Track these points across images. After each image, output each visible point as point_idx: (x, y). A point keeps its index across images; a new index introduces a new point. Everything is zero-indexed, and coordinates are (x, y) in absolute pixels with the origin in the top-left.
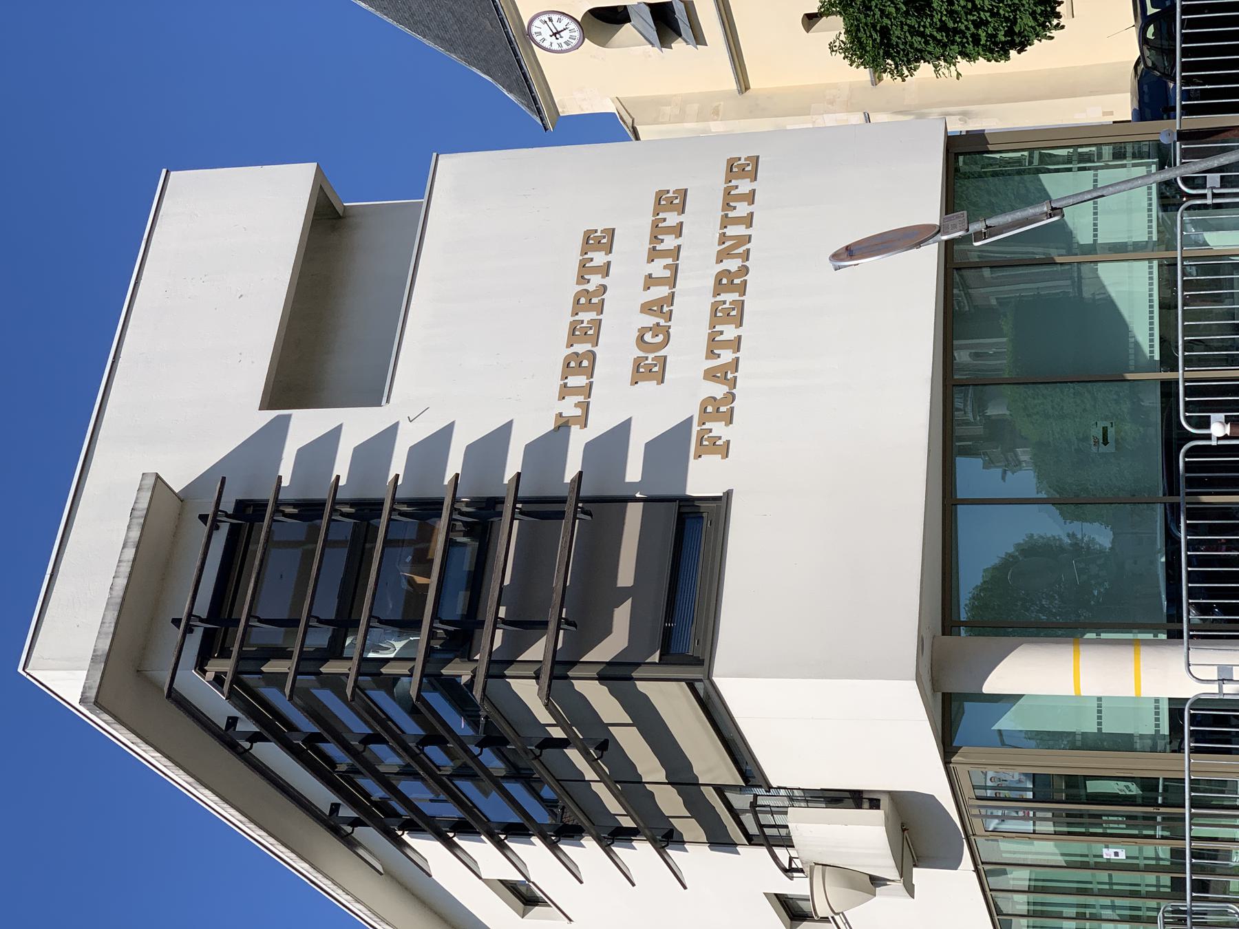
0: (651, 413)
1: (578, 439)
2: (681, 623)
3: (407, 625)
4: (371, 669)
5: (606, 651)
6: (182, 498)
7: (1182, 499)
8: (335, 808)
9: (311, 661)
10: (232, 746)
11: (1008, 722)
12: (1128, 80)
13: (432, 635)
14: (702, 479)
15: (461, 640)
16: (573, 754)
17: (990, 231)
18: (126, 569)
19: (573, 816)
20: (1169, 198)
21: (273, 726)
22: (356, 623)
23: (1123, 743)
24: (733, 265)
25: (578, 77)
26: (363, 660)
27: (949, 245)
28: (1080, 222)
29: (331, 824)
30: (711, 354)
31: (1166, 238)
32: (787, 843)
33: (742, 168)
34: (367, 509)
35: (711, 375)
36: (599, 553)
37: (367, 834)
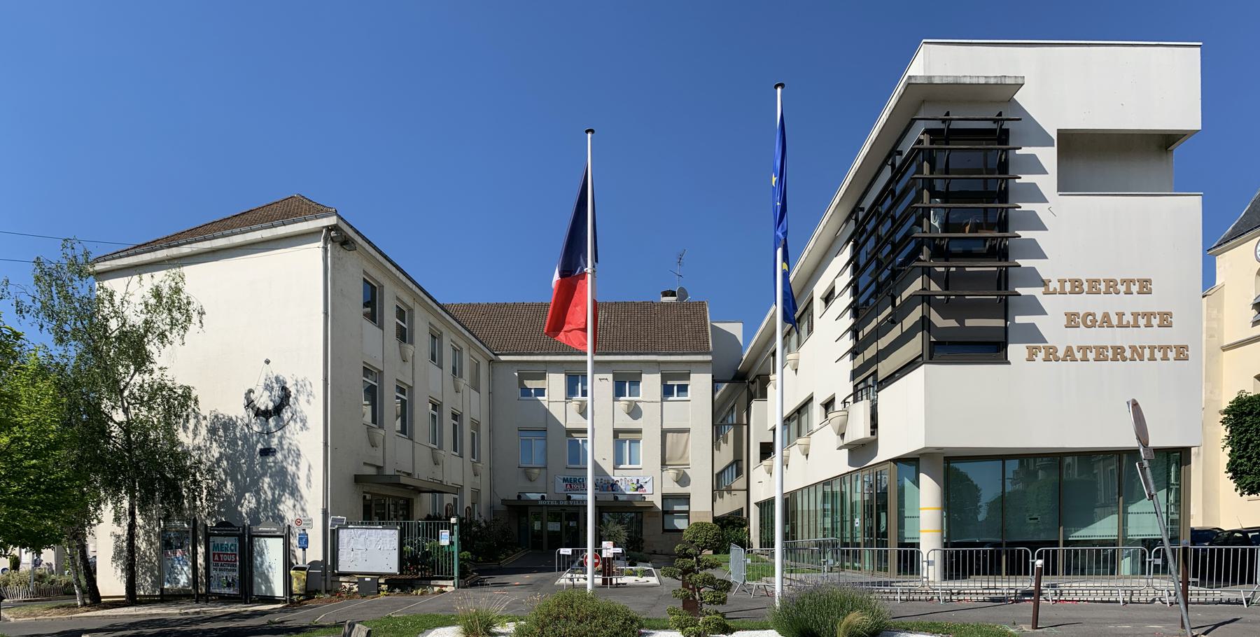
0: (1050, 325)
1: (1037, 292)
2: (946, 349)
3: (946, 226)
4: (926, 213)
5: (936, 318)
6: (1011, 101)
7: (1003, 549)
8: (862, 209)
9: (929, 185)
10: (889, 156)
11: (908, 483)
12: (1210, 525)
13: (941, 239)
14: (1016, 351)
15: (940, 252)
16: (889, 310)
17: (1143, 470)
18: (974, 81)
19: (862, 313)
20: (1149, 544)
21: (898, 173)
22: (947, 202)
23: (901, 525)
24: (1128, 354)
25: (1239, 265)
26: (929, 209)
27: (1137, 451)
28: (1144, 505)
29: (856, 209)
30: (1080, 348)
31: (1127, 542)
32: (855, 401)
33: (1182, 353)
34: (1003, 196)
35: (1069, 349)
36: (981, 310)
37: (852, 226)
